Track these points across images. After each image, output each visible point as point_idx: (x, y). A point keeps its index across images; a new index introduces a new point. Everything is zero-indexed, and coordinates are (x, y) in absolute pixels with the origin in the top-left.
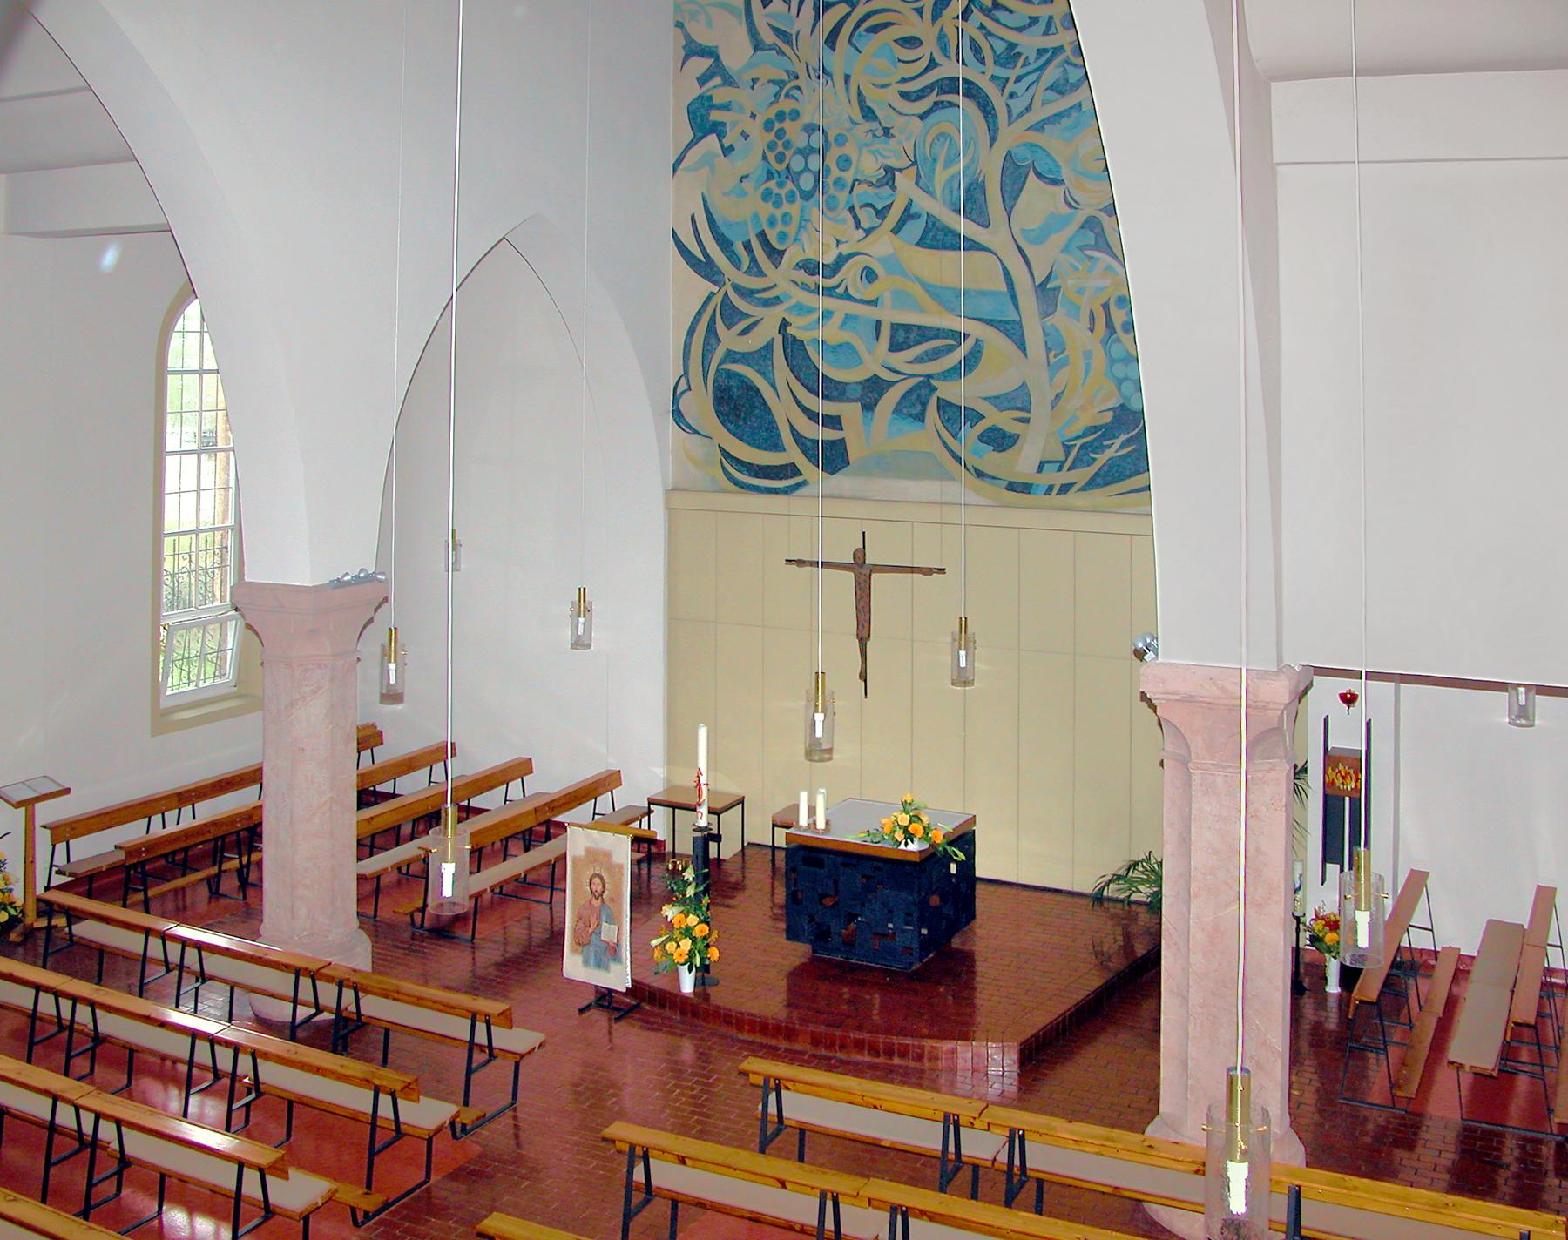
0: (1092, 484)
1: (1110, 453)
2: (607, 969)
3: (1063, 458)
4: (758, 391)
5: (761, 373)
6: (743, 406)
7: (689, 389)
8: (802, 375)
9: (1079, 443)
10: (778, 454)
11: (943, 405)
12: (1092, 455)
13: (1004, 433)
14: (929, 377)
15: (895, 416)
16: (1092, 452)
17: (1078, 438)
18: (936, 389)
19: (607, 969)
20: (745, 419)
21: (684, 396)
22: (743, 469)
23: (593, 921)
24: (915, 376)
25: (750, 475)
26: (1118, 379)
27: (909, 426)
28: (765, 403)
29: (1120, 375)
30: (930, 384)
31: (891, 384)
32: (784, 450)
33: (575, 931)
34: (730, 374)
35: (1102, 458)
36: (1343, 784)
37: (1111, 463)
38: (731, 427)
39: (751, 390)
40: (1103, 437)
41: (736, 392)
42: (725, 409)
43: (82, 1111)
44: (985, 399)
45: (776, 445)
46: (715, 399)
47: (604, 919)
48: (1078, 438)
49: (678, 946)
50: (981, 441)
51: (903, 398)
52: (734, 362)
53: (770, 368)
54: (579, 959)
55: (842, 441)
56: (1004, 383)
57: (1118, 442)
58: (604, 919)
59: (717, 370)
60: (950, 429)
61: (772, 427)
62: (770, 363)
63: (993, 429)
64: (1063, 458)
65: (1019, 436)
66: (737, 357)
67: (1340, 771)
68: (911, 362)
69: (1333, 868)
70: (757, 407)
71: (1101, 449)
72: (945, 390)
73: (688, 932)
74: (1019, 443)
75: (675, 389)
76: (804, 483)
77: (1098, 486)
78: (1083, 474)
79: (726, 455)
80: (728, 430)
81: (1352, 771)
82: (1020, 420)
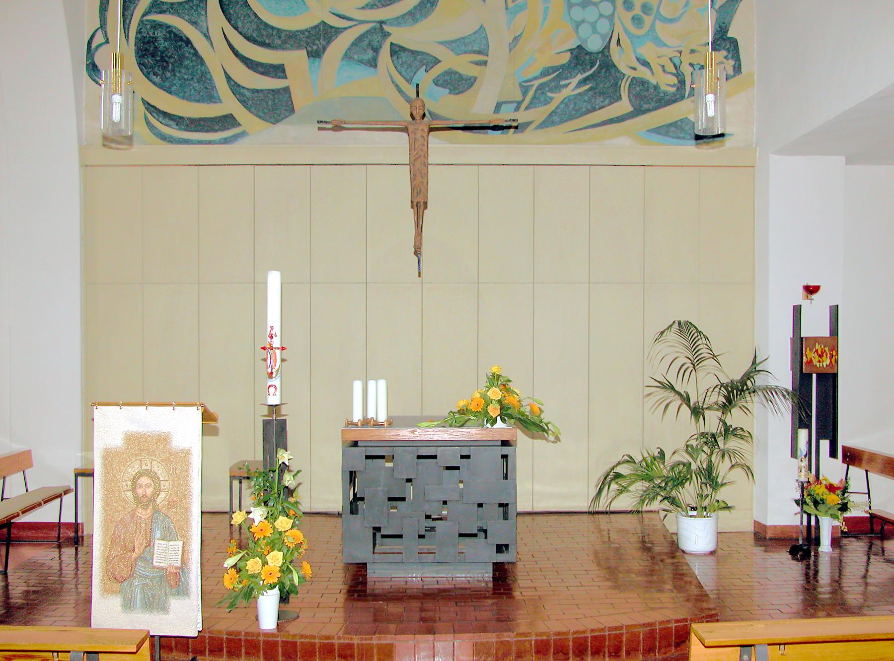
0: (548, 123)
1: (567, 92)
2: (164, 609)
3: (520, 98)
4: (188, 42)
5: (194, 23)
6: (170, 57)
7: (107, 41)
8: (240, 24)
9: (536, 83)
10: (212, 106)
11: (396, 50)
12: (549, 94)
13: (460, 75)
14: (382, 22)
15: (344, 62)
16: (549, 91)
17: (535, 78)
18: (389, 34)
19: (164, 609)
20: (173, 71)
21: (101, 50)
22: (171, 123)
23: (139, 542)
24: (368, 22)
25: (180, 129)
26: (575, 22)
27: (363, 72)
28: (196, 54)
29: (578, 18)
30: (382, 29)
31: (338, 31)
32: (221, 102)
33: (108, 560)
34: (156, 25)
35: (558, 97)
36: (819, 361)
37: (566, 102)
38: (157, 80)
39: (180, 40)
40: (559, 78)
41: (162, 44)
42: (149, 60)
43: (59, 500)
44: (442, 43)
45: (211, 97)
46: (137, 52)
47: (158, 535)
48: (535, 78)
49: (265, 563)
50: (436, 85)
51: (354, 44)
52: (161, 12)
53: (203, 17)
54: (116, 602)
55: (287, 90)
56: (464, 28)
57: (575, 81)
58: (158, 535)
59: (141, 22)
60: (404, 73)
61: (205, 78)
62: (203, 12)
63: (450, 73)
64: (520, 98)
65: (475, 78)
66: (165, 7)
67: (817, 351)
68: (363, 8)
69: (803, 434)
70: (187, 57)
71: (558, 88)
72: (400, 35)
73: (276, 542)
74: (476, 83)
75: (90, 43)
76: (243, 134)
77: (553, 123)
78: (539, 113)
79: (150, 107)
80: (154, 83)
81: (827, 349)
82: (477, 63)
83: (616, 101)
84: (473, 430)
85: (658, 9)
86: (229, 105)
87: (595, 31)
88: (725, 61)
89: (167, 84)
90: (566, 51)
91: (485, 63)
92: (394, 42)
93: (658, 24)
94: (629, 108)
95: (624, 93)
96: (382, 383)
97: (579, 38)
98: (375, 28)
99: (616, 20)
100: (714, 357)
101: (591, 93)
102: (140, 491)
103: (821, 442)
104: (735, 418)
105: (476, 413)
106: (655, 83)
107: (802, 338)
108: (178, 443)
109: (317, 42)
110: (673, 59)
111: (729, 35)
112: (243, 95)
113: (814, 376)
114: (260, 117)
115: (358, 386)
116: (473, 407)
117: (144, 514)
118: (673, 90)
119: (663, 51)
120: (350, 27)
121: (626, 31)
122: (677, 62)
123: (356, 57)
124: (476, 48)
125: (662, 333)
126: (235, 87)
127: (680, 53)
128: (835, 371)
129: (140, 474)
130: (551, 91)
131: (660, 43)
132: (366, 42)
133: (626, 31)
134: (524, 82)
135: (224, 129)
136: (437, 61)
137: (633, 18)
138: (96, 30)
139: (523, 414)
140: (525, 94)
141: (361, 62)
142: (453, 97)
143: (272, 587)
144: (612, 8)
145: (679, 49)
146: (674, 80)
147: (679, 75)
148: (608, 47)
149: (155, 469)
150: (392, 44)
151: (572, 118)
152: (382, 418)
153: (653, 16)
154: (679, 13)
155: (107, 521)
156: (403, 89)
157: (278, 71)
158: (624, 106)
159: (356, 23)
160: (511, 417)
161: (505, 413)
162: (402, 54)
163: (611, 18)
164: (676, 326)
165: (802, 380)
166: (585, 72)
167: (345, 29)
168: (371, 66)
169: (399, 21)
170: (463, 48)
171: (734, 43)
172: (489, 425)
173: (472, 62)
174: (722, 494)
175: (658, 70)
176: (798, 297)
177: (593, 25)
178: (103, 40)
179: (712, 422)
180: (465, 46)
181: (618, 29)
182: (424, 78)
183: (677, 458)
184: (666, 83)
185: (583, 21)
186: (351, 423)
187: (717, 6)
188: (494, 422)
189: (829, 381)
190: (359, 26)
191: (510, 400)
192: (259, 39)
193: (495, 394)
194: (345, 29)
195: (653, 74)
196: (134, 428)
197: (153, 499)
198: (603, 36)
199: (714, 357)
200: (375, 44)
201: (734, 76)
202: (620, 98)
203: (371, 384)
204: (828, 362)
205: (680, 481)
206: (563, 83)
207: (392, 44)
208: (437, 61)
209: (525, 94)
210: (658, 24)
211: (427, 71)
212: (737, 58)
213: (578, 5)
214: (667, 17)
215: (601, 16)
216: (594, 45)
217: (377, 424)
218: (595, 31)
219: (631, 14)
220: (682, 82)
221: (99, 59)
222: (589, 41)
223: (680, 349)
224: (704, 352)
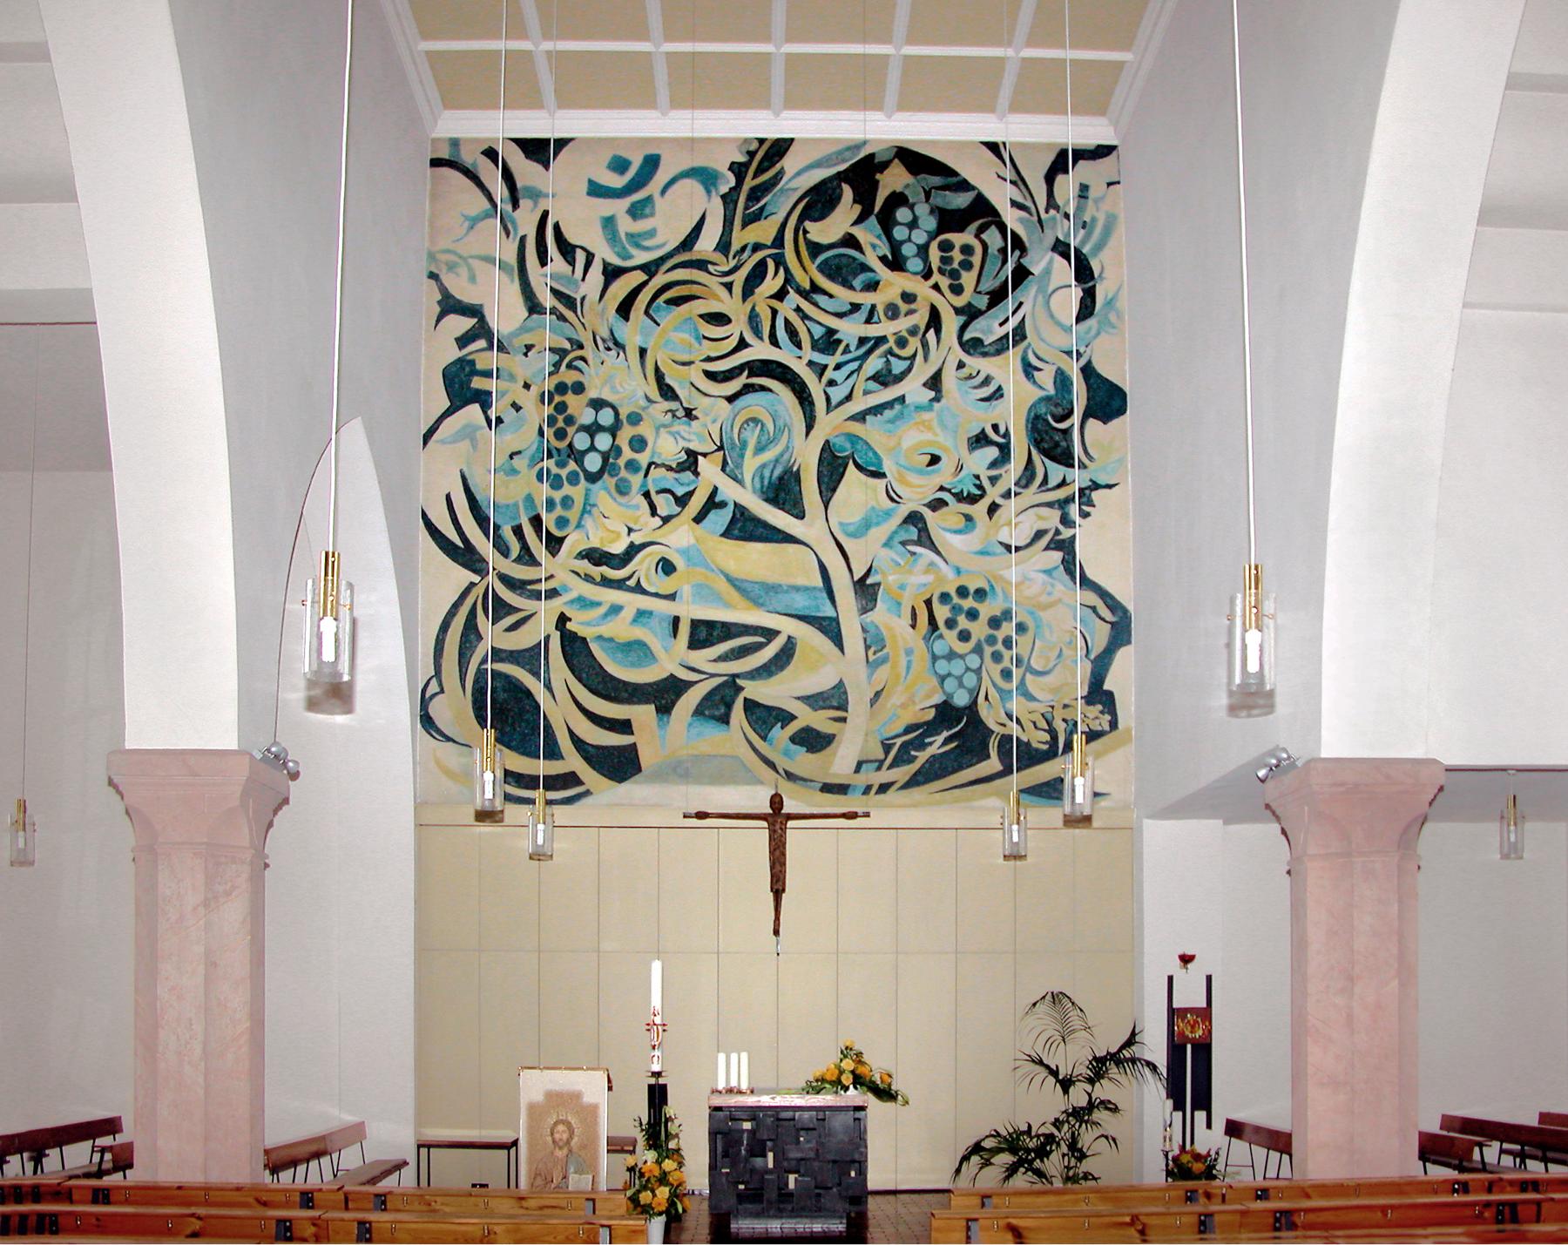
0: (912, 782)
1: (934, 750)
3: (882, 756)
7: (442, 691)
9: (899, 741)
11: (750, 705)
12: (913, 753)
14: (735, 676)
18: (742, 689)
20: (513, 724)
29: (942, 672)
31: (689, 685)
35: (922, 756)
36: (1192, 1032)
37: (933, 759)
44: (798, 698)
45: (553, 753)
47: (572, 1170)
49: (654, 1195)
56: (821, 681)
57: (940, 739)
58: (572, 1170)
64: (882, 756)
65: (834, 736)
68: (715, 661)
71: (922, 746)
76: (587, 793)
78: (903, 773)
83: (985, 760)
84: (829, 1097)
85: (1029, 660)
86: (573, 762)
87: (961, 685)
88: (1101, 715)
89: (506, 739)
90: (931, 707)
91: (844, 720)
92: (748, 697)
93: (1028, 676)
94: (998, 767)
95: (993, 752)
96: (744, 1056)
97: (944, 692)
98: (726, 682)
99: (984, 674)
100: (1087, 1028)
101: (958, 751)
102: (557, 1136)
103: (1196, 1113)
104: (1103, 1090)
105: (831, 1083)
106: (1026, 740)
107: (1174, 1009)
108: (588, 1099)
109: (666, 696)
110: (1046, 715)
111: (1106, 687)
112: (585, 751)
113: (1189, 1047)
114: (605, 776)
115: (722, 1057)
116: (828, 1077)
117: (560, 1154)
118: (1045, 747)
119: (1033, 705)
120: (701, 681)
121: (995, 685)
122: (1049, 716)
123: (707, 713)
124: (835, 704)
125: (1034, 1004)
126: (578, 742)
127: (1053, 707)
128: (1208, 1041)
129: (556, 1124)
130: (916, 750)
131: (1030, 697)
132: (718, 698)
133: (995, 685)
134: (887, 739)
135: (565, 787)
136: (793, 717)
137: (1002, 671)
138: (430, 679)
139: (874, 1082)
140: (887, 753)
141: (713, 717)
142: (811, 756)
143: (660, 1214)
144: (979, 661)
145: (1052, 704)
146: (1047, 737)
147: (1053, 733)
148: (975, 702)
149: (569, 1118)
150: (745, 699)
151: (938, 777)
152: (744, 1086)
153: (1024, 668)
154: (1051, 665)
155: (530, 1161)
156: (757, 747)
157: (624, 726)
158: (993, 764)
159: (704, 676)
160: (862, 1084)
161: (858, 1080)
162: (757, 711)
163: (978, 671)
164: (1049, 997)
165: (1175, 1050)
166: (951, 729)
167: (696, 682)
168: (723, 722)
169: (755, 674)
170: (821, 703)
171: (1110, 695)
172: (842, 1092)
173: (831, 719)
174: (1085, 1166)
175: (1029, 726)
176: (1175, 967)
177: (960, 679)
178: (438, 690)
179: (1078, 1096)
180: (824, 701)
181: (986, 682)
182: (781, 735)
183: (1043, 1130)
184: (1039, 739)
185: (949, 675)
186: (715, 1091)
187: (1092, 657)
188: (846, 1089)
189: (1204, 1050)
190: (712, 680)
191: (861, 1070)
192: (603, 692)
193: (848, 1065)
194: (696, 682)
195: (1024, 730)
196: (550, 1087)
197: (568, 1142)
198: (970, 691)
199: (1087, 1028)
200: (728, 699)
201: (1111, 731)
202: (988, 757)
203: (734, 1056)
204: (1201, 1032)
205: (1042, 1153)
206: (927, 740)
207: (745, 699)
208: (793, 717)
209: (887, 753)
210: (1028, 676)
211: (782, 728)
212: (1113, 713)
213: (943, 657)
214: (1041, 670)
215: (968, 669)
216: (961, 699)
217: (740, 1092)
218: (961, 685)
219: (1000, 667)
220: (1054, 738)
221: (435, 709)
222: (955, 695)
223: (1048, 1020)
224: (1076, 1023)
